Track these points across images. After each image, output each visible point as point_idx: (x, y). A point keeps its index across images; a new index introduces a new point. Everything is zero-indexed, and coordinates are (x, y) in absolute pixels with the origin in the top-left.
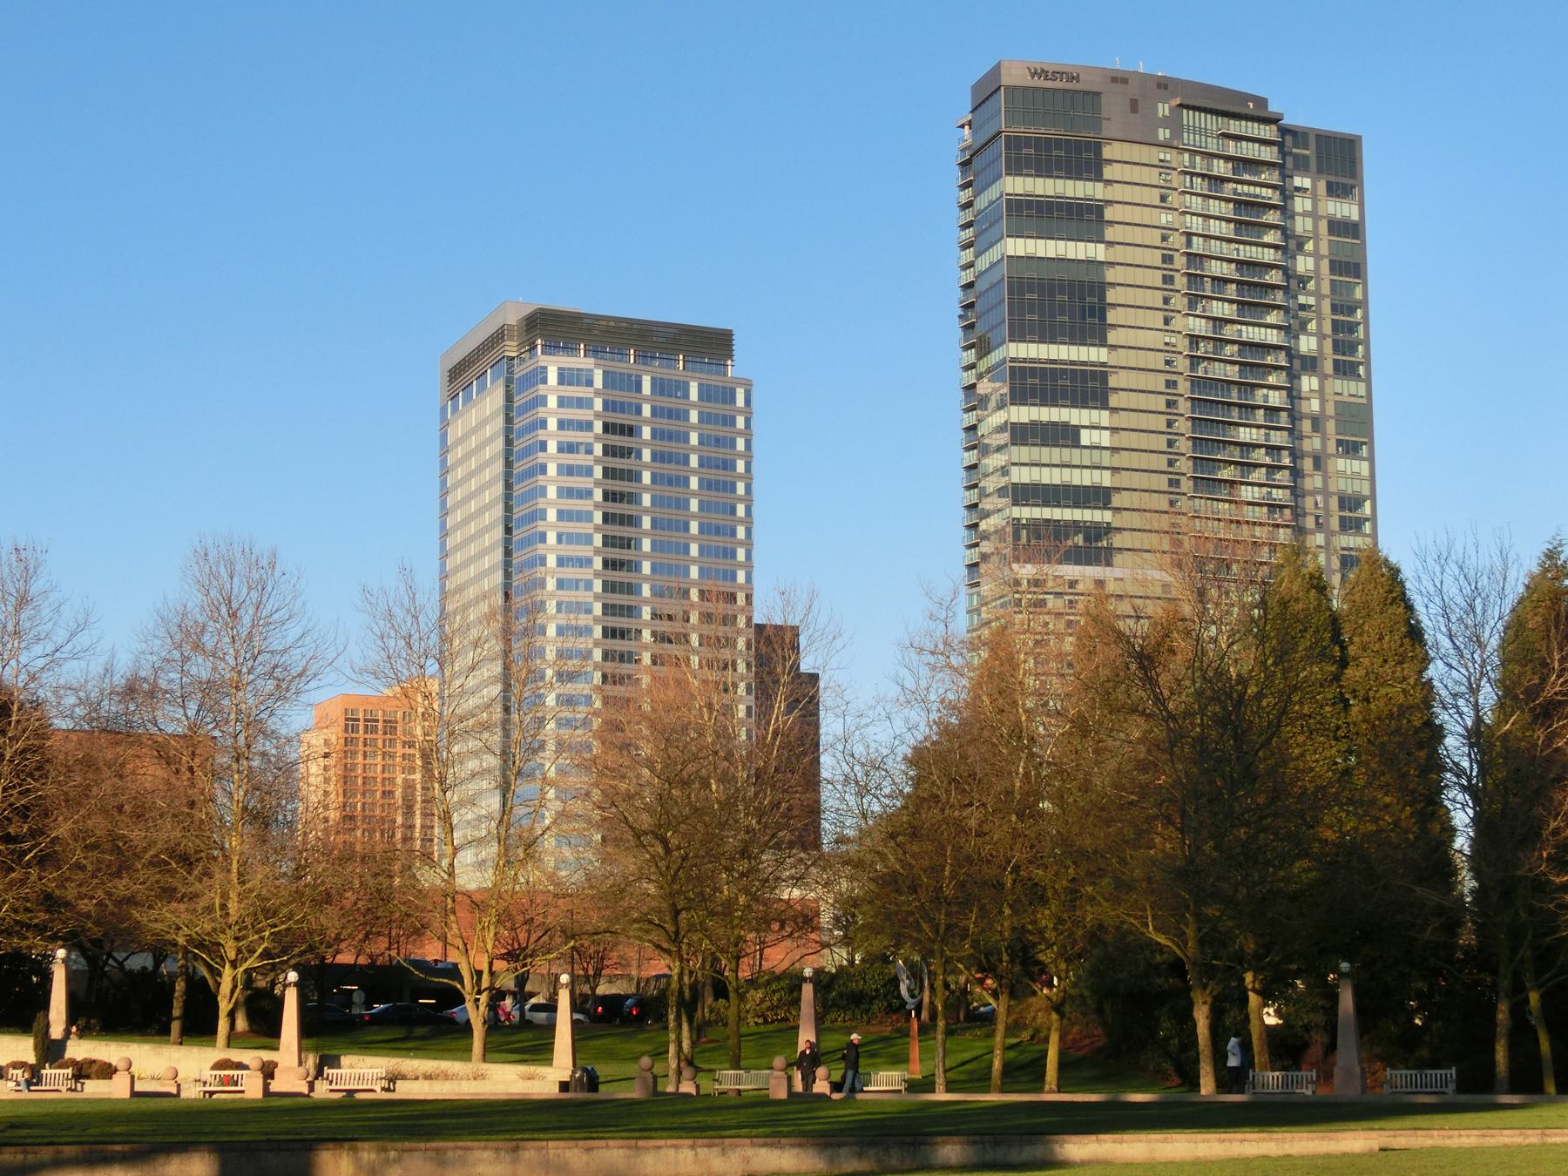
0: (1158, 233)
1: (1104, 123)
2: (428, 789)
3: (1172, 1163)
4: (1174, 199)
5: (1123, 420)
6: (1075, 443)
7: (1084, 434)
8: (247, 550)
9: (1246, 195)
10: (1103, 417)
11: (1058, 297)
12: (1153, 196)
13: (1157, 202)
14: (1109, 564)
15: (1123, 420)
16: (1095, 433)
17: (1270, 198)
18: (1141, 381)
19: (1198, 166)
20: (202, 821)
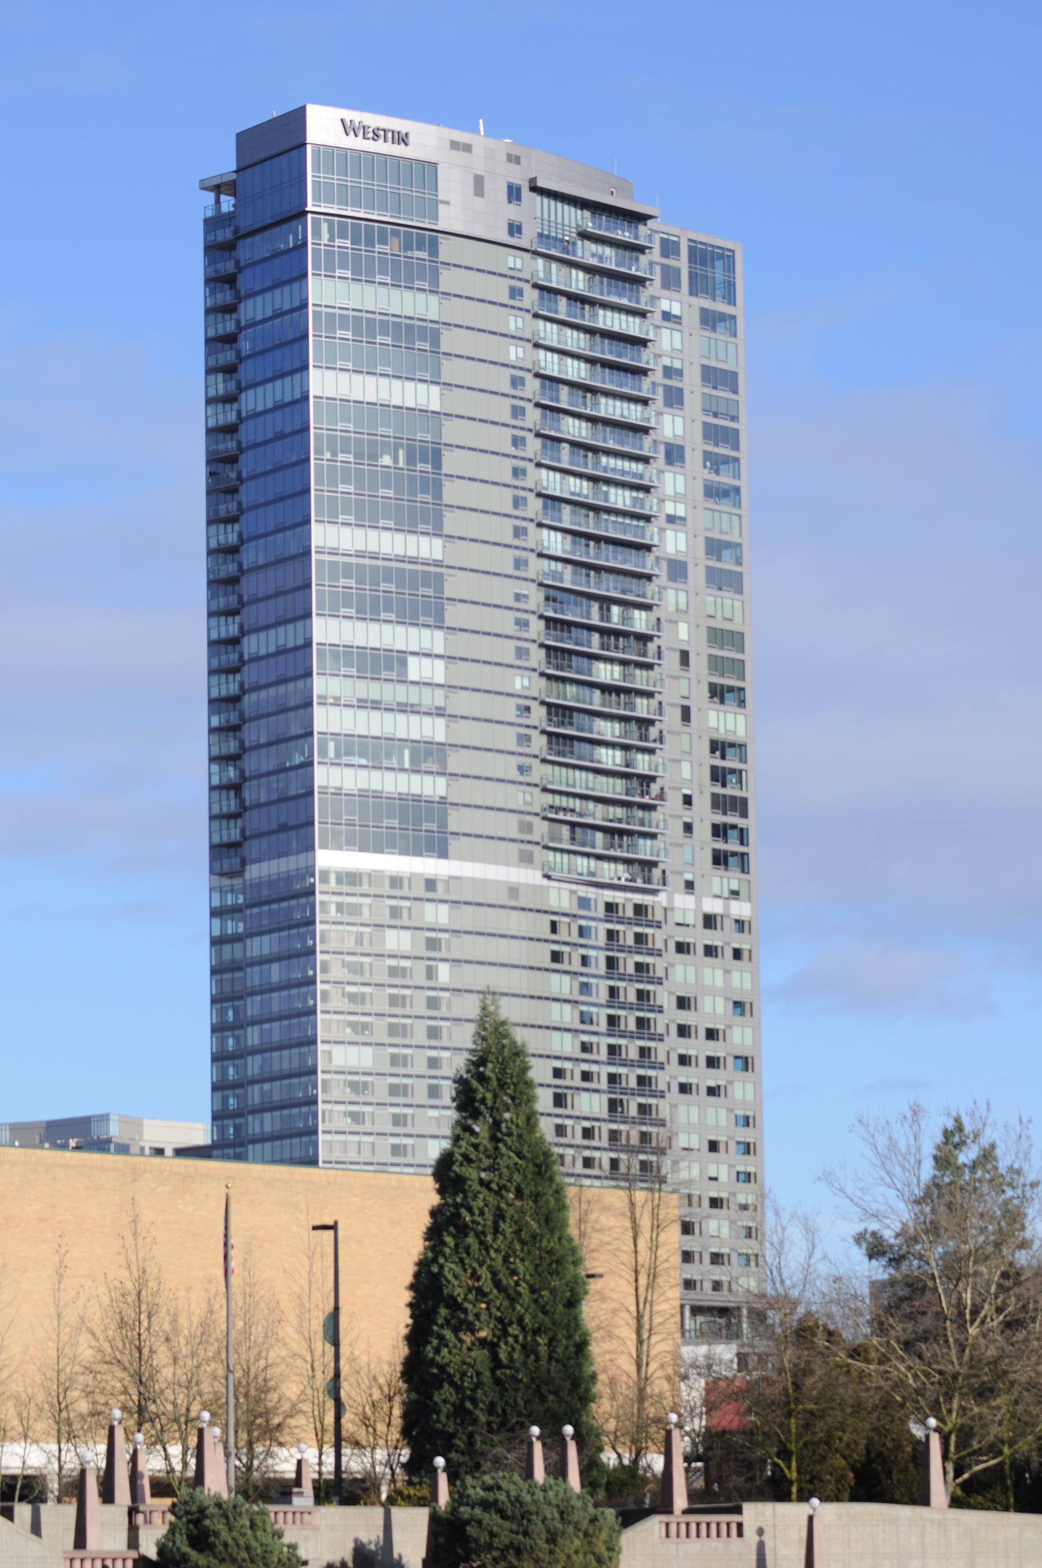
0: (507, 373)
1: (442, 208)
3: (414, 1505)
5: (467, 646)
9: (614, 470)
10: (436, 640)
13: (510, 658)
14: (443, 854)
15: (467, 646)
17: (620, 821)
19: (554, 278)
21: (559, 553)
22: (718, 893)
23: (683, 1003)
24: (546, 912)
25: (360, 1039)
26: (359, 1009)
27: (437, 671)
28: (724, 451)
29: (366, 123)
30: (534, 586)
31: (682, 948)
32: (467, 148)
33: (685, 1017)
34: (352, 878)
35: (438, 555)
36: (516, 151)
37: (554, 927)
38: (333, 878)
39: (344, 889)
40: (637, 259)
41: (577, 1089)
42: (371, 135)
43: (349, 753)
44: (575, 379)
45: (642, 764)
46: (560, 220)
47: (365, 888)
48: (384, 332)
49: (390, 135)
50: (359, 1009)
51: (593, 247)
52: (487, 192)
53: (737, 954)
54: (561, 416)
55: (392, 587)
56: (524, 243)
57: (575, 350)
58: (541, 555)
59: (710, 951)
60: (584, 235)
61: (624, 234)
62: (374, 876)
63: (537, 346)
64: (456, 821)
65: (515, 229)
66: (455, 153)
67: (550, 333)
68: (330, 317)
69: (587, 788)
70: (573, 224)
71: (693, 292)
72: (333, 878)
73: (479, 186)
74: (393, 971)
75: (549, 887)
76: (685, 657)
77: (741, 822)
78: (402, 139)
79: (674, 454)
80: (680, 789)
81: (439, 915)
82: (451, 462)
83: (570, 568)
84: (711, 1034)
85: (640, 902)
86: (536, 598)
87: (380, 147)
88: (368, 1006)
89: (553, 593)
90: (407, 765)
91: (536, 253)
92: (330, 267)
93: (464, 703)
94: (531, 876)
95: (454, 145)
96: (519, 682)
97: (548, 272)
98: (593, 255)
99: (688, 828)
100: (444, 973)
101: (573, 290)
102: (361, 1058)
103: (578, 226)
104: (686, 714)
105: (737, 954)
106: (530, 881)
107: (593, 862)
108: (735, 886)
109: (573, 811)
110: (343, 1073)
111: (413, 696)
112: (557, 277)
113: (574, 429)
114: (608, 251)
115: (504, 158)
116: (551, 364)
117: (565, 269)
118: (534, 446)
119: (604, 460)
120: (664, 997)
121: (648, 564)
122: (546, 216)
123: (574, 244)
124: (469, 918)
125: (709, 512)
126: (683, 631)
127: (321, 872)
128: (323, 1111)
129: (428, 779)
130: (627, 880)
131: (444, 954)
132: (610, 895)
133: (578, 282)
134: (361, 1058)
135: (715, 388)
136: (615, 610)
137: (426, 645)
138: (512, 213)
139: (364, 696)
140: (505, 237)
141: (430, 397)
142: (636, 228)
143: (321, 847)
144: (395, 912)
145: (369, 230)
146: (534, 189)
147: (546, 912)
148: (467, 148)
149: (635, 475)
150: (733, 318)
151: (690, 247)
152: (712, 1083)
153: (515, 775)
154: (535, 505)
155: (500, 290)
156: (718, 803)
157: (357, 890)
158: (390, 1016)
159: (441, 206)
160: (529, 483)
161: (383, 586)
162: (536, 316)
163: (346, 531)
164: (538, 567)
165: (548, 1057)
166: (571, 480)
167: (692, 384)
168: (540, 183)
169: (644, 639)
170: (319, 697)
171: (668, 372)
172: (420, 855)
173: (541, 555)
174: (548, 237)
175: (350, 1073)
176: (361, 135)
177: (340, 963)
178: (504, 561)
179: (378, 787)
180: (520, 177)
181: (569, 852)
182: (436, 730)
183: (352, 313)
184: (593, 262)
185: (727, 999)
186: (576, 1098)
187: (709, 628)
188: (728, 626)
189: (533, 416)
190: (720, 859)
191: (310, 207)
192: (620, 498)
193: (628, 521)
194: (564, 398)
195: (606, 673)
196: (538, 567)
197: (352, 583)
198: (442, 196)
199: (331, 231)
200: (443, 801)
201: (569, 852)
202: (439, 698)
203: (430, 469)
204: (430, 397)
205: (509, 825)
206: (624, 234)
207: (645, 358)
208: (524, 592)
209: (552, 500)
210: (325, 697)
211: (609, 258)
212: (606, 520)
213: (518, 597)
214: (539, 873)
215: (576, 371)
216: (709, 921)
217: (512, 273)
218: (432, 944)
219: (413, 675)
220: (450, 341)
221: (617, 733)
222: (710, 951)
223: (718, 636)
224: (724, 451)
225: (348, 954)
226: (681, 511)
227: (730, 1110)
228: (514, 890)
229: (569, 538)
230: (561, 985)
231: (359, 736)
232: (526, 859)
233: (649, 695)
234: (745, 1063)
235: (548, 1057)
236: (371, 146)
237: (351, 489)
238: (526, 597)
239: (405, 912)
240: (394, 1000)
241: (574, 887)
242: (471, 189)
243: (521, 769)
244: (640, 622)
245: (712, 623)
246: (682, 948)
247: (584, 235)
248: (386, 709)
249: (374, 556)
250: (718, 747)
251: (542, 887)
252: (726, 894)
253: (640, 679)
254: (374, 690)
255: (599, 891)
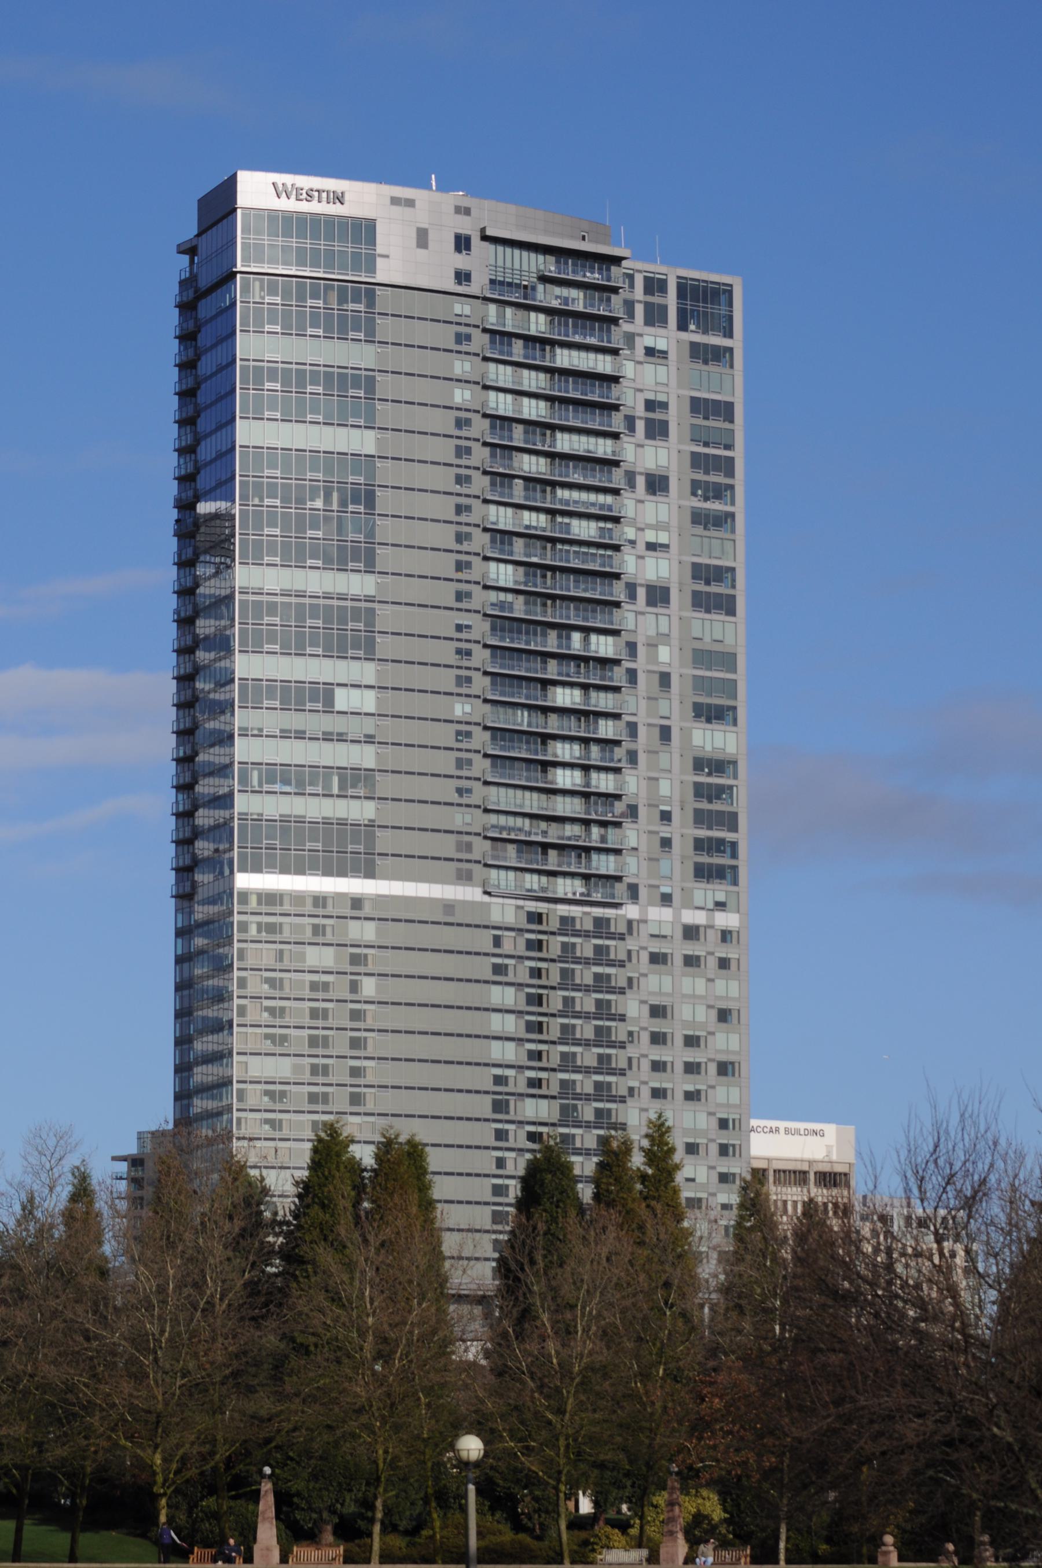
1: (379, 261)
2: (163, 1302)
4: (479, 793)
6: (329, 700)
7: (340, 694)
8: (57, 1156)
10: (368, 672)
11: (309, 622)
12: (446, 790)
16: (355, 693)
18: (405, 504)
20: (77, 1249)
21: (510, 585)
22: (702, 905)
23: (657, 1011)
24: (486, 927)
25: (278, 1050)
26: (278, 1022)
27: (368, 701)
28: (716, 478)
29: (298, 185)
30: (479, 616)
31: (657, 959)
32: (410, 203)
33: (658, 1025)
34: (271, 898)
35: (371, 591)
36: (466, 202)
37: (497, 941)
38: (253, 900)
39: (264, 909)
40: (609, 300)
41: (521, 1095)
42: (304, 196)
43: (271, 780)
44: (534, 418)
45: (603, 783)
46: (517, 266)
47: (287, 907)
48: (273, 378)
49: (324, 195)
50: (278, 1022)
51: (558, 290)
52: (431, 244)
53: (724, 964)
54: (514, 453)
55: (320, 623)
56: (474, 288)
57: (533, 389)
58: (486, 587)
59: (691, 961)
60: (544, 279)
61: (593, 277)
62: (298, 898)
63: (486, 387)
64: (384, 841)
65: (463, 277)
66: (397, 210)
67: (503, 375)
68: (258, 370)
69: (515, 805)
70: (534, 269)
71: (682, 326)
72: (253, 900)
73: (422, 238)
74: (314, 986)
75: (489, 904)
76: (665, 679)
77: (730, 836)
78: (339, 199)
79: (657, 484)
80: (657, 806)
81: (368, 932)
82: (385, 500)
83: (521, 598)
84: (691, 1041)
85: (566, 914)
86: (481, 628)
87: (314, 207)
88: (287, 1019)
89: (502, 622)
90: (335, 790)
91: (486, 299)
92: (259, 323)
93: (393, 730)
94: (472, 893)
95: (395, 201)
96: (460, 709)
97: (501, 316)
98: (557, 297)
99: (666, 843)
100: (369, 987)
101: (533, 332)
102: (280, 1068)
103: (539, 271)
104: (665, 733)
105: (724, 964)
106: (469, 898)
107: (544, 879)
108: (721, 897)
109: (520, 830)
110: (259, 1082)
111: (337, 724)
112: (511, 320)
113: (532, 465)
114: (574, 293)
115: (452, 210)
116: (503, 404)
117: (521, 313)
118: (480, 483)
119: (560, 492)
120: (633, 1007)
121: (618, 591)
122: (500, 263)
123: (534, 288)
124: (399, 934)
125: (698, 539)
126: (664, 654)
127: (239, 894)
128: (239, 1120)
129: (355, 804)
130: (582, 894)
131: (370, 968)
132: (563, 909)
133: (538, 324)
134: (280, 1068)
135: (706, 418)
136: (576, 637)
137: (355, 678)
138: (461, 261)
139: (329, 729)
140: (451, 285)
141: (365, 442)
142: (608, 270)
143: (239, 871)
144: (317, 930)
145: (301, 288)
146: (485, 238)
147: (486, 927)
148: (410, 203)
149: (602, 507)
150: (731, 350)
151: (678, 283)
152: (690, 1088)
153: (455, 798)
154: (480, 541)
155: (445, 336)
156: (700, 818)
157: (278, 909)
158: (352, 1029)
159: (379, 260)
160: (474, 518)
161: (309, 622)
162: (486, 359)
163: (314, 575)
164: (481, 598)
165: (486, 1065)
166: (526, 514)
167: (676, 417)
168: (489, 233)
169: (605, 663)
170: (240, 729)
171: (651, 405)
172: (303, 873)
173: (486, 587)
174: (502, 283)
175: (266, 1083)
176: (293, 197)
177: (258, 979)
178: (446, 594)
179: (301, 812)
180: (467, 226)
181: (516, 869)
182: (366, 757)
183: (364, 373)
184: (555, 304)
185: (709, 1007)
186: (519, 1104)
187: (694, 650)
188: (717, 647)
189: (480, 455)
190: (703, 873)
191: (239, 267)
192: (584, 529)
193: (593, 551)
194: (518, 436)
195: (564, 697)
196: (481, 598)
197: (320, 623)
198: (380, 249)
199: (262, 289)
200: (371, 825)
201: (516, 869)
202: (369, 726)
203: (362, 510)
204: (365, 442)
205: (447, 846)
206: (593, 277)
207: (614, 394)
208: (466, 623)
209: (506, 536)
210: (246, 729)
211: (578, 299)
212: (561, 550)
213: (459, 628)
214: (479, 891)
215: (533, 410)
216: (691, 932)
217: (458, 319)
218: (355, 960)
219: (340, 704)
220: (386, 386)
221: (577, 754)
222: (691, 961)
223: (702, 657)
224: (716, 478)
225: (266, 970)
226: (663, 538)
227: (710, 1114)
228: (449, 906)
229: (521, 570)
230: (505, 996)
231: (366, 770)
232: (464, 878)
233: (617, 716)
234: (724, 1069)
235: (486, 1065)
236: (304, 207)
237: (278, 531)
238: (468, 627)
239: (329, 930)
240: (314, 1014)
241: (521, 903)
242: (413, 242)
243: (460, 791)
244: (603, 646)
245: (698, 645)
246: (657, 959)
247: (544, 279)
248: (352, 741)
249: (342, 597)
250: (700, 764)
251: (482, 903)
252: (711, 905)
253: (602, 701)
254: (295, 720)
255: (552, 906)
